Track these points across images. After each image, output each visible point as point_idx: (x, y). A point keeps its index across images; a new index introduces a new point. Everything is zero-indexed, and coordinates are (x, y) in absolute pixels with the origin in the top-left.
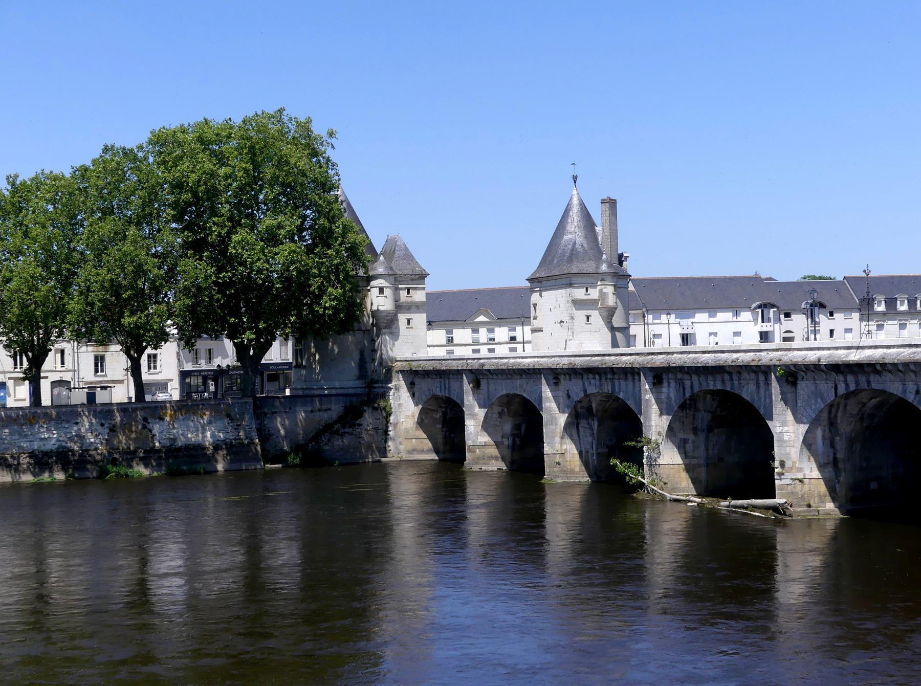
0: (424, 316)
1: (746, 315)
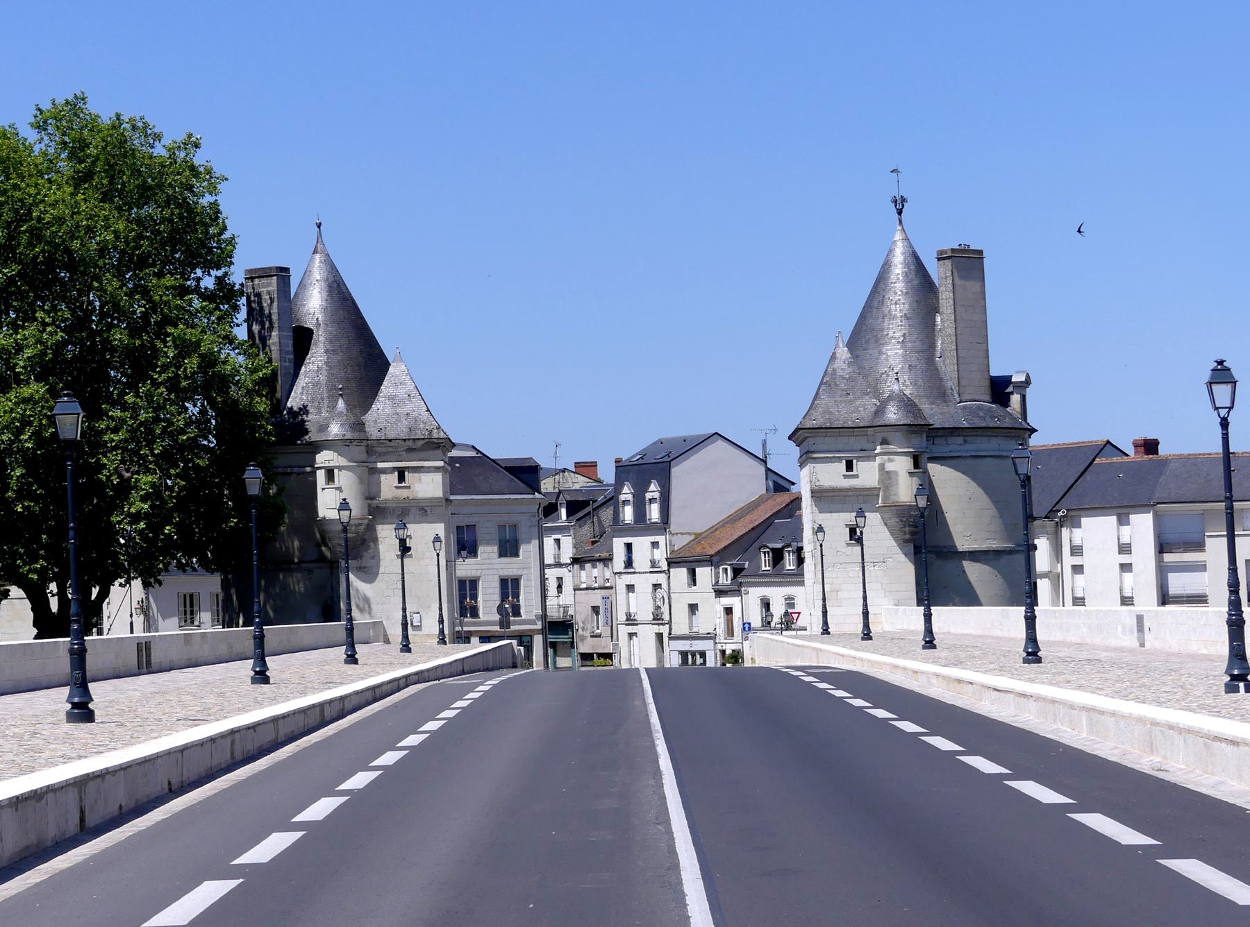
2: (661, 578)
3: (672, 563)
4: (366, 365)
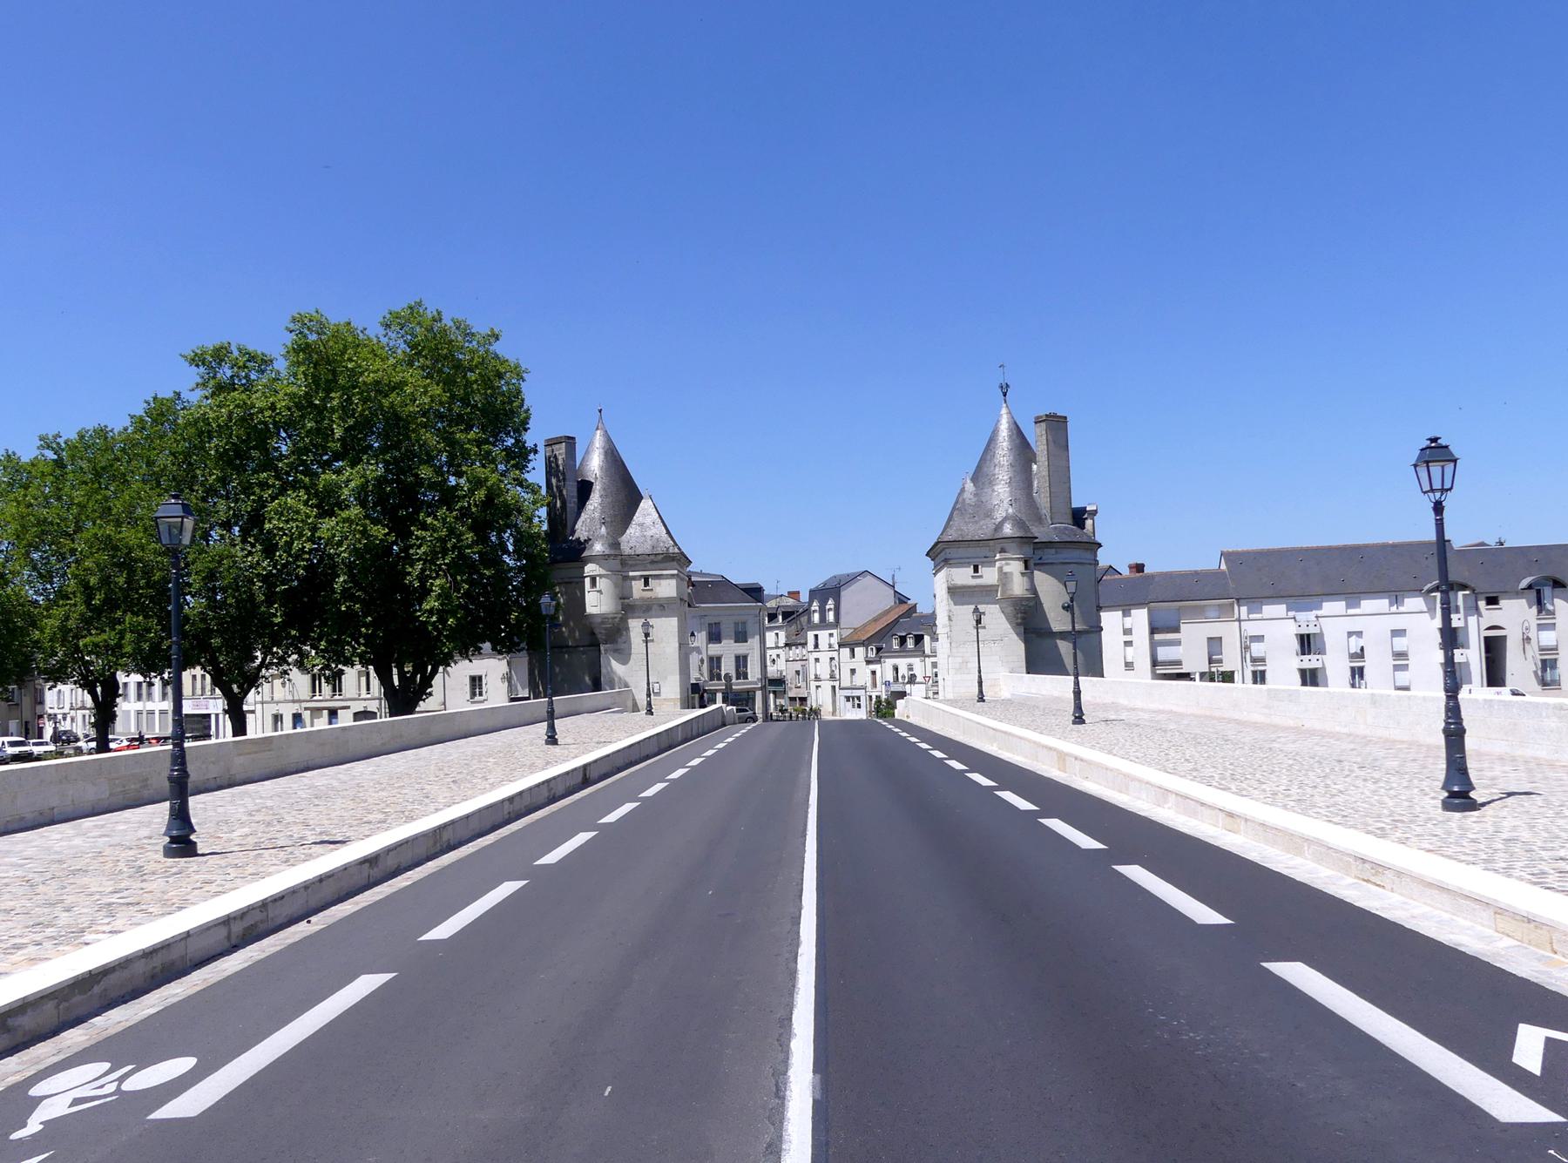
0: (674, 621)
1: (1415, 603)
2: (835, 654)
3: (840, 645)
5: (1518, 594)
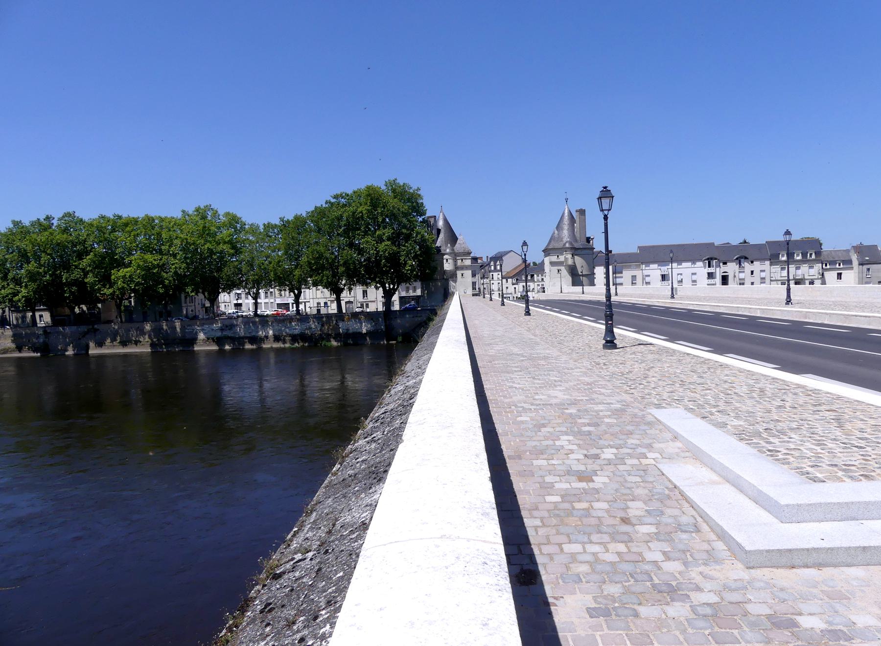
0: (470, 272)
4: (453, 238)
5: (732, 261)
